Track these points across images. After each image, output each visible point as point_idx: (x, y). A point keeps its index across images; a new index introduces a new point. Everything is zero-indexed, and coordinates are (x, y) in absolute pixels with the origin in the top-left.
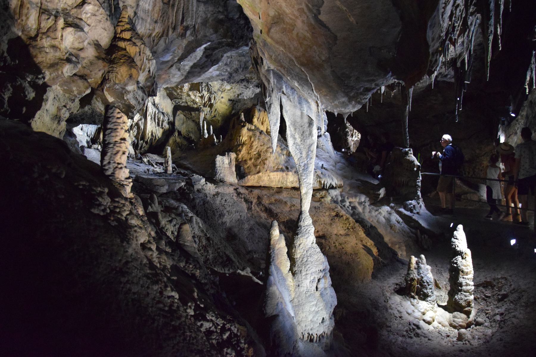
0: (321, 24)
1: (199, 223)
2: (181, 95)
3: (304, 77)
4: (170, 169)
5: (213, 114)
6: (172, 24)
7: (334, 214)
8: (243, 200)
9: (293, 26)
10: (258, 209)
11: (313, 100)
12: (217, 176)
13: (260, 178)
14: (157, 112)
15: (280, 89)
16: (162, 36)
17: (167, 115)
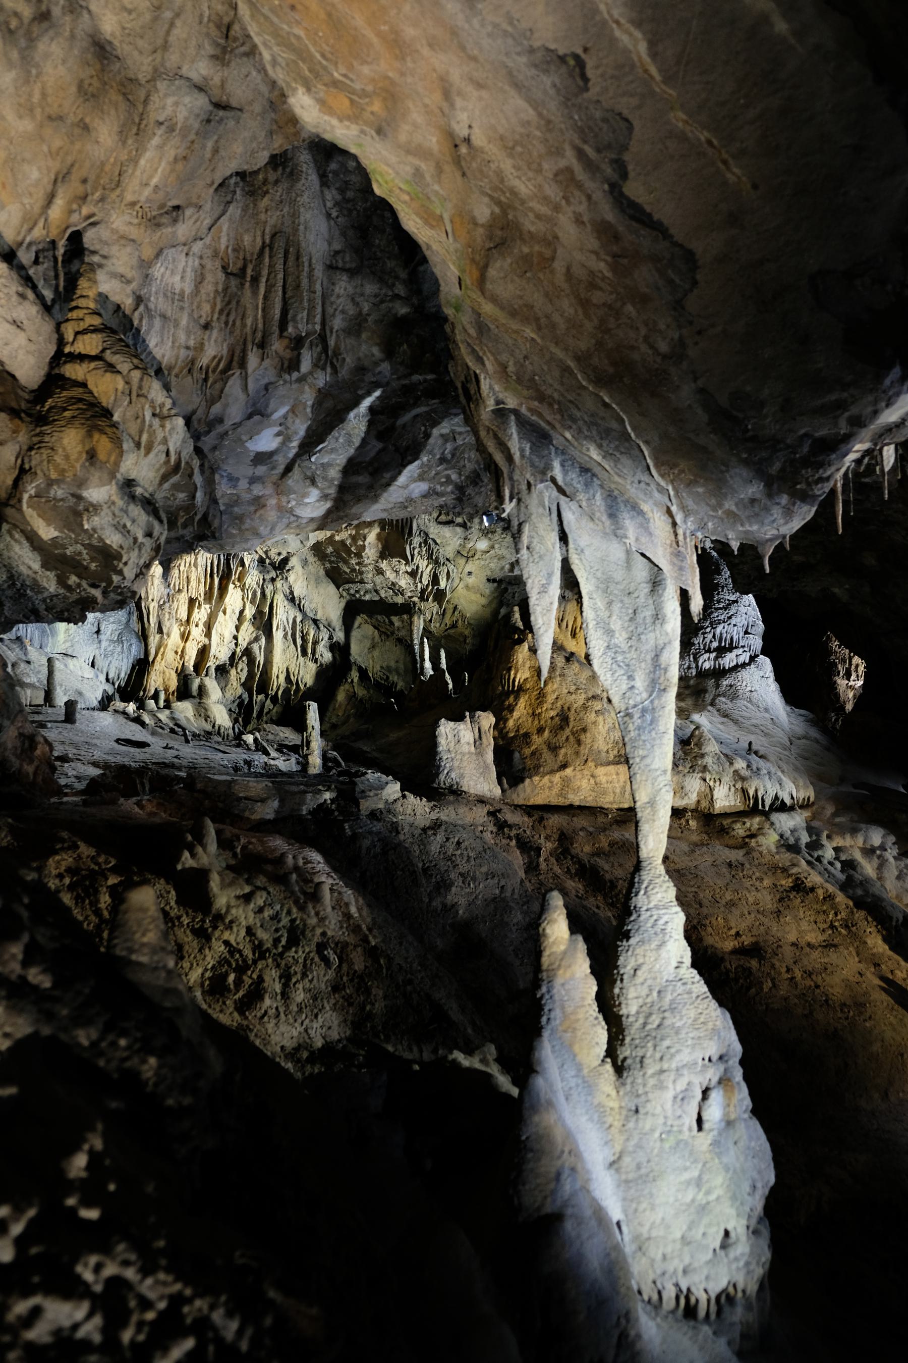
0: (636, 214)
1: (347, 905)
2: (361, 573)
3: (614, 425)
4: (316, 761)
5: (447, 620)
6: (254, 332)
7: (787, 883)
8: (514, 843)
9: (549, 244)
10: (557, 870)
11: (656, 504)
12: (442, 777)
13: (566, 782)
14: (298, 620)
15: (543, 473)
16: (228, 367)
17: (329, 626)
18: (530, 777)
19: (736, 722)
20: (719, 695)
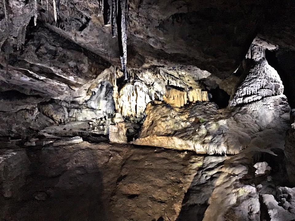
18: (139, 138)
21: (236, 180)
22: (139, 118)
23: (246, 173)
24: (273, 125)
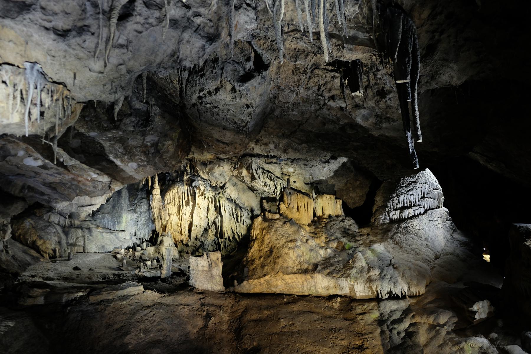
18: (247, 280)
19: (401, 247)
20: (398, 233)
21: (448, 333)
22: (191, 246)
23: (456, 320)
24: (449, 250)
